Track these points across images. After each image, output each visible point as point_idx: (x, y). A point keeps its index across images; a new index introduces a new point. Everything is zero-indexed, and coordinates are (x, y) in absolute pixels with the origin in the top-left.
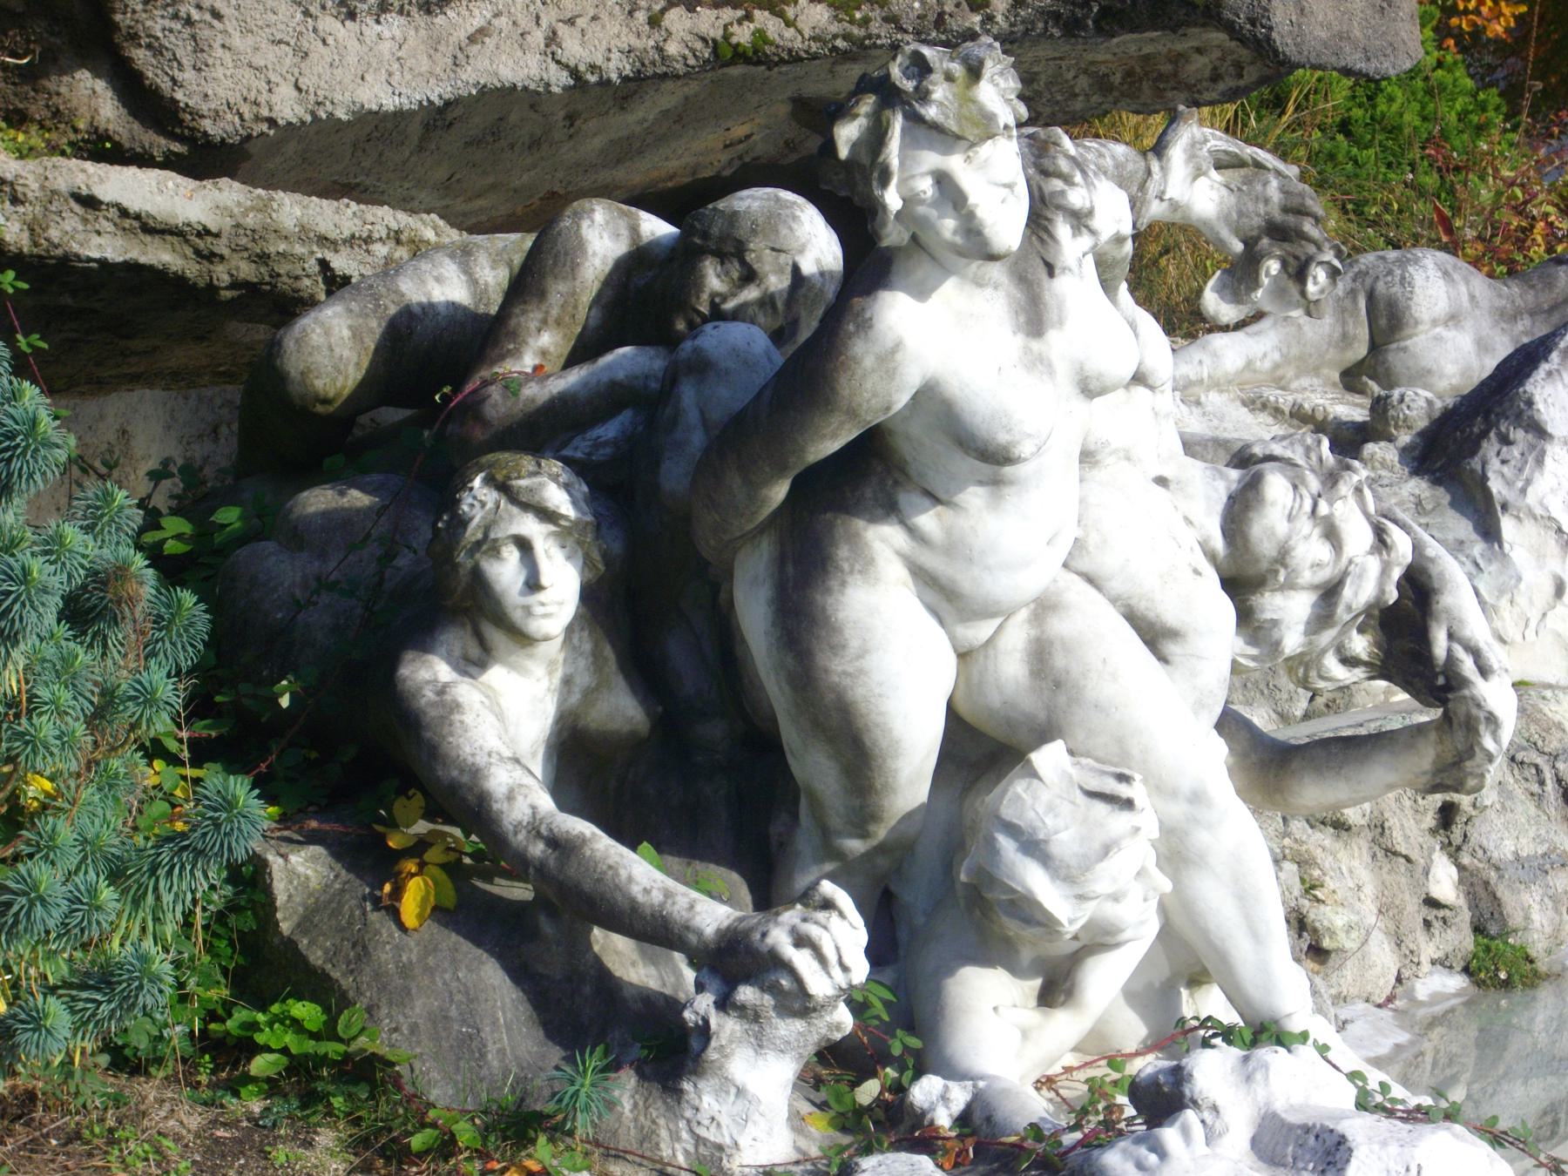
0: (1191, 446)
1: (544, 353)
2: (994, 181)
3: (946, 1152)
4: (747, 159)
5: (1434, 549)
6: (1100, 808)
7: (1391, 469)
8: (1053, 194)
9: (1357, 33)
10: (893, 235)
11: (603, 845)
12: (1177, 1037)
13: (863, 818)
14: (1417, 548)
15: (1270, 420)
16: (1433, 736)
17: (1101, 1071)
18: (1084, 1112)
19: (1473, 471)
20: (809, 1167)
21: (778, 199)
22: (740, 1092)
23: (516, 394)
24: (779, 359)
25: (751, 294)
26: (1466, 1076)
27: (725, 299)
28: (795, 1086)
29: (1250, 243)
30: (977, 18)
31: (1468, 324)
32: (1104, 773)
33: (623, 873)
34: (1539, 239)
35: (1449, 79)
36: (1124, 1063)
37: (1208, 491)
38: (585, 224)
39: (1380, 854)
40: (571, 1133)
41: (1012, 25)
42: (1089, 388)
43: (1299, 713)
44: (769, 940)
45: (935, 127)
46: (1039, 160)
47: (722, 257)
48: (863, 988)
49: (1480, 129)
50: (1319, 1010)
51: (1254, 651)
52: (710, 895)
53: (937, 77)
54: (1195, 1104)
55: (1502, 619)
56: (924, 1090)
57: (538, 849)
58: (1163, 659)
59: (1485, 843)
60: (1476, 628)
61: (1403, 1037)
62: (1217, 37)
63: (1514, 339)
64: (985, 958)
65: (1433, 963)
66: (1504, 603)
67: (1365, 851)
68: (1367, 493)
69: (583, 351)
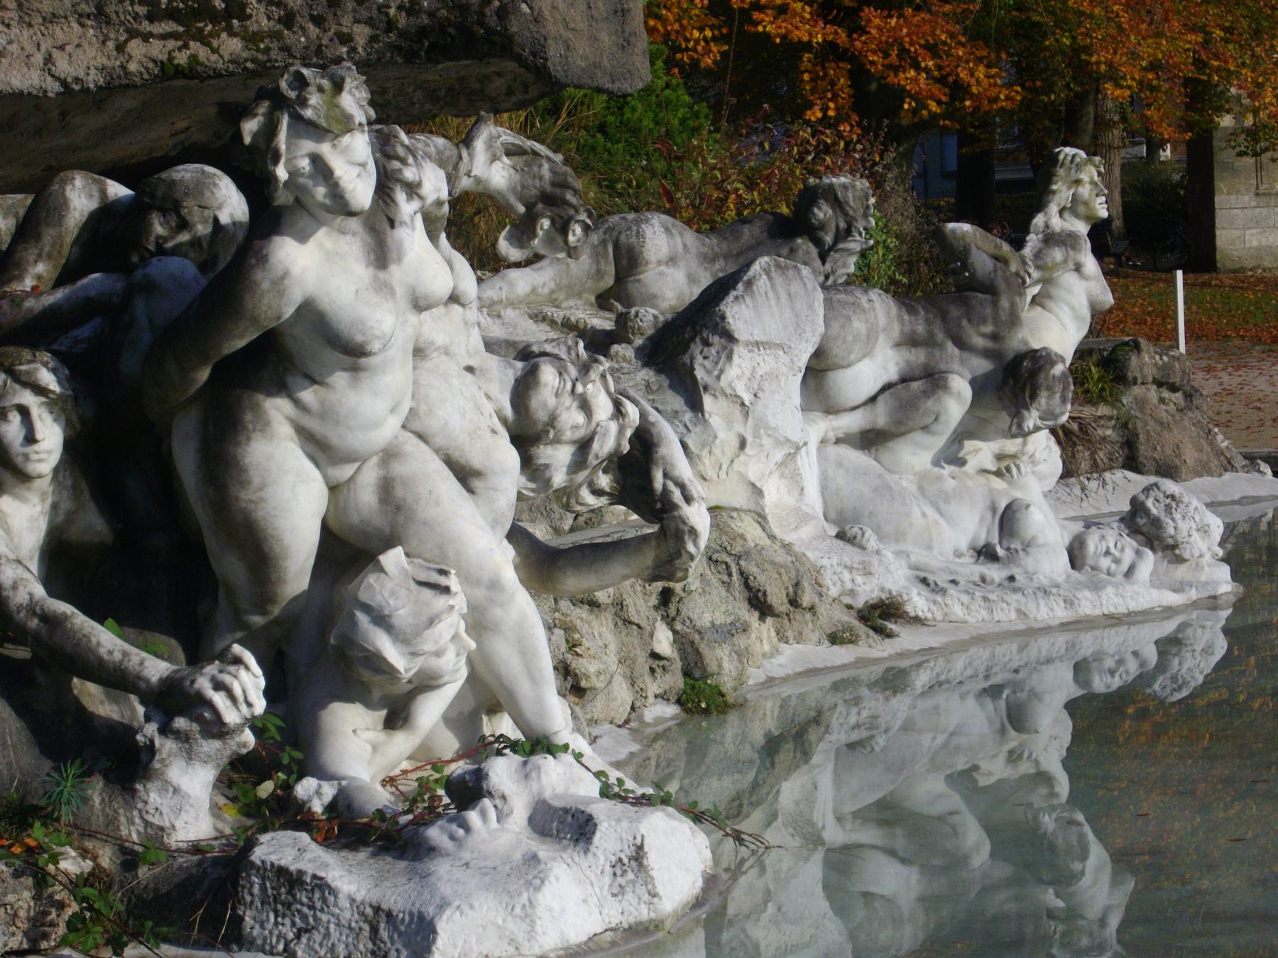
0: (491, 346)
1: (39, 277)
2: (353, 164)
3: (319, 830)
4: (187, 144)
5: (654, 416)
6: (427, 593)
7: (629, 362)
8: (393, 171)
9: (606, 63)
10: (283, 198)
11: (80, 620)
12: (479, 748)
13: (264, 598)
14: (643, 415)
15: (548, 328)
16: (653, 543)
17: (427, 772)
18: (414, 801)
19: (684, 364)
20: (224, 841)
21: (203, 172)
22: (176, 790)
23: (19, 306)
24: (204, 281)
25: (184, 237)
26: (679, 774)
27: (166, 240)
28: (215, 786)
29: (530, 206)
30: (345, 49)
31: (682, 264)
32: (429, 569)
33: (94, 640)
34: (732, 206)
35: (674, 96)
36: (443, 767)
37: (501, 375)
38: (68, 188)
39: (620, 623)
40: (58, 820)
41: (369, 54)
42: (419, 304)
43: (567, 528)
44: (196, 686)
45: (311, 124)
46: (384, 149)
47: (164, 211)
48: (262, 717)
49: (696, 131)
50: (578, 729)
51: (533, 486)
52: (156, 655)
53: (312, 89)
54: (490, 794)
55: (704, 464)
56: (306, 788)
57: (34, 623)
58: (471, 491)
59: (691, 616)
60: (683, 469)
61: (635, 747)
62: (510, 65)
63: (713, 274)
64: (347, 696)
65: (656, 696)
66: (705, 453)
67: (610, 620)
68: (609, 378)
69: (66, 276)
